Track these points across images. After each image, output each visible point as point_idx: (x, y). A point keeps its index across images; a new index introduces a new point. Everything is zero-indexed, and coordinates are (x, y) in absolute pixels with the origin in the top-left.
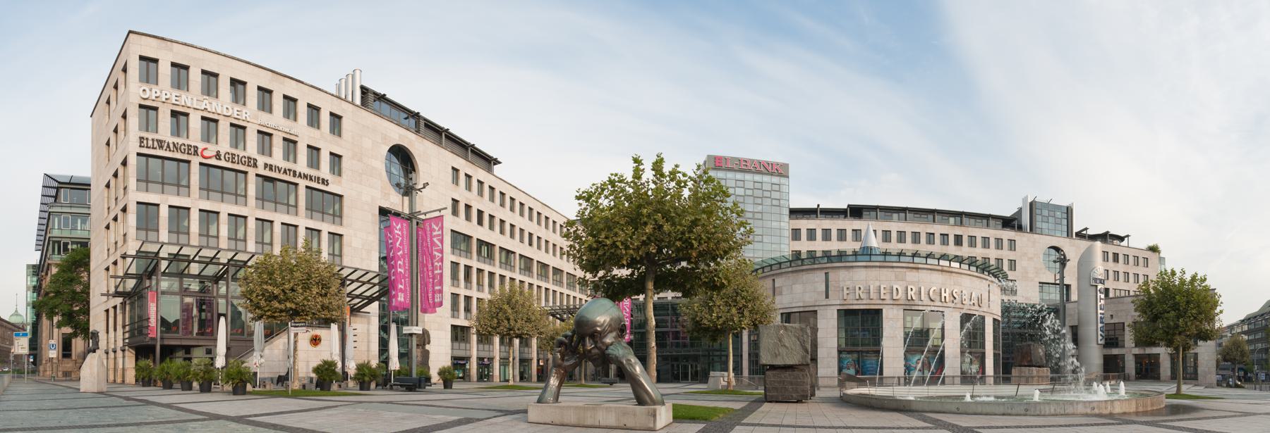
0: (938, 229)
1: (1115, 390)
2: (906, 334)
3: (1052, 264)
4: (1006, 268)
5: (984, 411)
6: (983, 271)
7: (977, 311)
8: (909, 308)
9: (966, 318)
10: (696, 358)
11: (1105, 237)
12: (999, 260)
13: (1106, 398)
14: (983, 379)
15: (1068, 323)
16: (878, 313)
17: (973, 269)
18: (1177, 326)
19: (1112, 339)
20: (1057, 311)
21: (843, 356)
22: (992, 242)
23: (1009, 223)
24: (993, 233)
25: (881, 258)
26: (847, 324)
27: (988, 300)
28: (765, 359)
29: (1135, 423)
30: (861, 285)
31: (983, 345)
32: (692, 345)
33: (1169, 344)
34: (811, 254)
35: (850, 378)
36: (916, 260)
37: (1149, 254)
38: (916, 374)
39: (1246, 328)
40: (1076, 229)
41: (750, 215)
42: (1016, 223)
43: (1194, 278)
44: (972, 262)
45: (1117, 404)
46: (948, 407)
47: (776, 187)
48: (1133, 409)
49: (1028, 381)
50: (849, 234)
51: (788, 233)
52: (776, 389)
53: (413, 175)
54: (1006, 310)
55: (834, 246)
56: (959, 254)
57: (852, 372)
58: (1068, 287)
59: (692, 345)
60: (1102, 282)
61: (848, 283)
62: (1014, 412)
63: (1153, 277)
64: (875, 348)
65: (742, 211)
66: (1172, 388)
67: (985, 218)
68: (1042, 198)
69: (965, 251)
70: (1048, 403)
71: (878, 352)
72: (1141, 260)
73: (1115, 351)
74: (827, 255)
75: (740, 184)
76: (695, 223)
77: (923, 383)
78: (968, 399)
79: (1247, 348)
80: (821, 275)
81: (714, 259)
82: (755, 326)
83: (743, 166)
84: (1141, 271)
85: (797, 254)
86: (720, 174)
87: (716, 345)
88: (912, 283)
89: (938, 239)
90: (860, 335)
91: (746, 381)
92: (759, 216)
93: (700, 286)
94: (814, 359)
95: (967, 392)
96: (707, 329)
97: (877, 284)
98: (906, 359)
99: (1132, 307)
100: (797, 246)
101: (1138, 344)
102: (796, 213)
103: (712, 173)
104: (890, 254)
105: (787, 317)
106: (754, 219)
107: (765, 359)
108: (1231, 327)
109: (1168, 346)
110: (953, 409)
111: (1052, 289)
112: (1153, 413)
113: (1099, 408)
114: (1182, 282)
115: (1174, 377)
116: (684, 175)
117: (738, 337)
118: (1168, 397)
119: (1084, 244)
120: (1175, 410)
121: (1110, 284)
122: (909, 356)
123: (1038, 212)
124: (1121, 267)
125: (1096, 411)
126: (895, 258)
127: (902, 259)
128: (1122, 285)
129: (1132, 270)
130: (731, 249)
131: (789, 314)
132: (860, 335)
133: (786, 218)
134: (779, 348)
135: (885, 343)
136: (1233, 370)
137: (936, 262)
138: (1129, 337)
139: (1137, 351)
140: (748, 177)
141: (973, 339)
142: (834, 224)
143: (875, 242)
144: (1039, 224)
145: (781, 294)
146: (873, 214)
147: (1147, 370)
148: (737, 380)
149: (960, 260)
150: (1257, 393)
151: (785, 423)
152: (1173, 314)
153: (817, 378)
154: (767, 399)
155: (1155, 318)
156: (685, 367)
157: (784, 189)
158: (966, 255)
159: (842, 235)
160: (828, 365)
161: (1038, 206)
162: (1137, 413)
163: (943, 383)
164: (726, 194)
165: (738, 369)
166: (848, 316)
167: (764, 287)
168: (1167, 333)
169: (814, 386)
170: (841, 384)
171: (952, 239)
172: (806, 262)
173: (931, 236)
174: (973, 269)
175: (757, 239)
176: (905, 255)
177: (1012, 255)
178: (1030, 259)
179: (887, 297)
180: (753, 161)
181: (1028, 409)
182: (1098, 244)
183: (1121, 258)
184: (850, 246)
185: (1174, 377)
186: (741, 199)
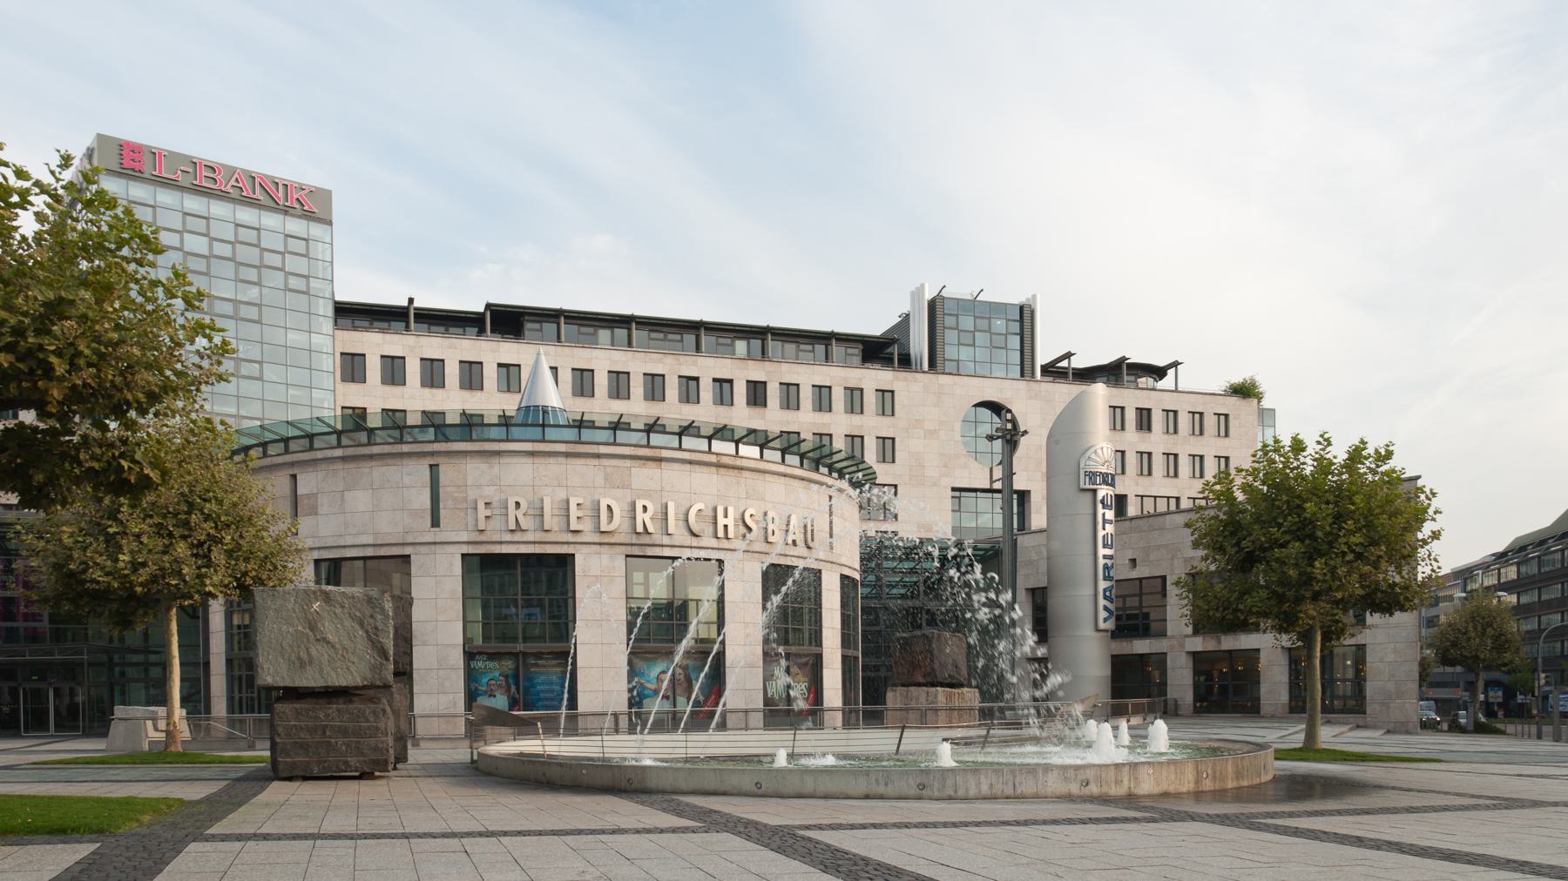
0: (708, 367)
1: (1139, 738)
2: (633, 613)
3: (984, 444)
4: (871, 456)
5: (821, 789)
6: (817, 464)
7: (801, 560)
8: (640, 551)
9: (774, 576)
10: (71, 671)
11: (1115, 372)
12: (855, 439)
13: (1121, 756)
14: (815, 713)
15: (1022, 583)
16: (564, 562)
17: (793, 460)
18: (1308, 580)
19: (1134, 614)
20: (990, 556)
21: (479, 664)
22: (838, 396)
23: (878, 350)
24: (841, 375)
25: (571, 434)
26: (487, 588)
27: (830, 533)
28: (272, 672)
29: (1193, 817)
30: (522, 497)
31: (817, 638)
32: (58, 636)
33: (1286, 623)
34: (395, 421)
35: (496, 718)
36: (656, 439)
37: (1233, 405)
38: (656, 706)
39: (1511, 573)
40: (1043, 357)
41: (228, 308)
43: (1356, 455)
44: (790, 444)
45: (1146, 772)
46: (733, 781)
47: (294, 245)
48: (1187, 785)
49: (925, 718)
50: (490, 374)
51: (330, 363)
52: (304, 747)
54: (873, 554)
55: (452, 401)
56: (757, 425)
57: (500, 702)
58: (1023, 496)
59: (58, 636)
60: (1108, 480)
61: (490, 492)
62: (890, 790)
63: (1242, 458)
64: (558, 646)
65: (200, 295)
66: (1295, 734)
67: (822, 342)
68: (959, 289)
69: (773, 418)
70: (975, 769)
71: (564, 657)
72: (1210, 422)
73: (1141, 646)
74: (434, 422)
75: (200, 225)
76: (56, 309)
77: (674, 726)
78: (781, 761)
79: (1513, 627)
81: (119, 412)
82: (244, 590)
83: (205, 180)
84: (1210, 446)
85: (356, 418)
86: (138, 191)
87: (133, 637)
88: (646, 494)
89: (707, 391)
90: (518, 615)
91: (221, 728)
92: (252, 313)
93: (77, 481)
94: (404, 673)
95: (779, 748)
96: (101, 596)
97: (562, 495)
98: (632, 672)
99: (1187, 537)
100: (355, 395)
101: (1202, 624)
103: (111, 185)
104: (592, 425)
105: (332, 570)
106: (235, 317)
107: (272, 672)
108: (1464, 575)
109: (1281, 629)
110: (747, 783)
111: (984, 502)
112: (1239, 795)
113: (1100, 781)
114: (1323, 466)
115: (1298, 705)
116: (21, 174)
117: (195, 618)
118: (1281, 755)
119: (1064, 392)
120: (1299, 788)
121: (1129, 485)
122: (639, 664)
123: (949, 321)
124: (1157, 441)
125: (1094, 789)
126: (605, 435)
127: (622, 436)
128: (1160, 485)
129: (1185, 446)
130: (168, 389)
131: (336, 564)
132: (518, 615)
133: (328, 325)
134: (309, 642)
135: (583, 634)
136: (1471, 687)
137: (702, 444)
138: (1177, 612)
139: (1198, 644)
140: (219, 209)
141: (793, 626)
142: (453, 349)
143: (554, 396)
144: (950, 352)
145: (314, 511)
146: (550, 328)
147: (1225, 690)
148: (195, 727)
149: (762, 440)
150: (1546, 746)
151: (328, 828)
152: (1296, 547)
153: (411, 720)
154: (277, 772)
155: (1247, 562)
156: (38, 696)
157: (319, 251)
158: (774, 429)
159: (472, 375)
160: (439, 686)
161: (949, 308)
162: (1198, 795)
163: (722, 726)
164: (151, 245)
165: (196, 699)
166: (490, 572)
167: (266, 492)
168: (1281, 598)
169: (404, 738)
170: (474, 731)
171: (740, 391)
172: (380, 436)
173: (690, 385)
174: (793, 460)
175: (246, 369)
176: (627, 427)
177: (885, 427)
178: (931, 434)
179: (587, 526)
180: (232, 170)
181: (926, 783)
182: (1100, 390)
183: (1157, 419)
184: (492, 402)
185: (1298, 705)
186: (193, 264)
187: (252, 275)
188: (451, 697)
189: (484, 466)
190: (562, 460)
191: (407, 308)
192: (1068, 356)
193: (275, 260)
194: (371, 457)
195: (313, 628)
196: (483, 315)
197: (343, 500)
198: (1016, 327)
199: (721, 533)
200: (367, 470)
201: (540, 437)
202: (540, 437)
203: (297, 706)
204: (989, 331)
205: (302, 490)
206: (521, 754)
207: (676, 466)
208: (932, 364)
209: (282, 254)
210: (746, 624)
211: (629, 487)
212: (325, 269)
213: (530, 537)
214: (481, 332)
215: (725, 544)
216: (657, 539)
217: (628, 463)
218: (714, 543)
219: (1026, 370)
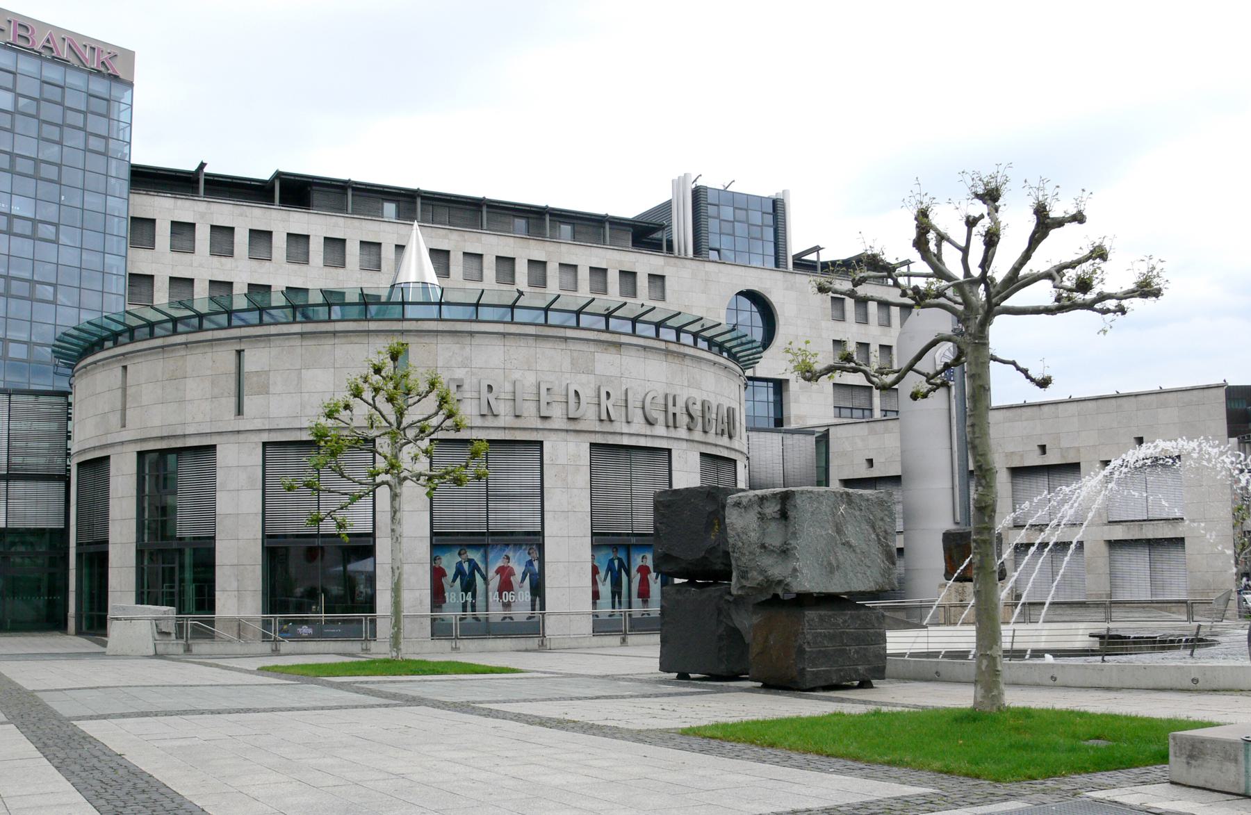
17: (703, 344)
23: (646, 233)
24: (615, 258)
40: (796, 244)
53: (629, 238)
67: (591, 227)
68: (712, 181)
75: (54, 93)
92: (51, 172)
102: (147, 179)
123: (712, 210)
142: (243, 217)
144: (714, 241)
145: (264, 390)
187: (54, 133)
188: (417, 593)
189: (456, 348)
190: (531, 341)
192: (817, 249)
193: (78, 120)
194: (335, 333)
195: (839, 531)
197: (300, 378)
198: (769, 219)
201: (436, 316)
202: (436, 316)
203: (822, 613)
205: (248, 367)
207: (633, 352)
208: (697, 251)
209: (85, 113)
211: (592, 372)
213: (501, 422)
215: (673, 433)
216: (617, 427)
217: (592, 348)
219: (779, 262)
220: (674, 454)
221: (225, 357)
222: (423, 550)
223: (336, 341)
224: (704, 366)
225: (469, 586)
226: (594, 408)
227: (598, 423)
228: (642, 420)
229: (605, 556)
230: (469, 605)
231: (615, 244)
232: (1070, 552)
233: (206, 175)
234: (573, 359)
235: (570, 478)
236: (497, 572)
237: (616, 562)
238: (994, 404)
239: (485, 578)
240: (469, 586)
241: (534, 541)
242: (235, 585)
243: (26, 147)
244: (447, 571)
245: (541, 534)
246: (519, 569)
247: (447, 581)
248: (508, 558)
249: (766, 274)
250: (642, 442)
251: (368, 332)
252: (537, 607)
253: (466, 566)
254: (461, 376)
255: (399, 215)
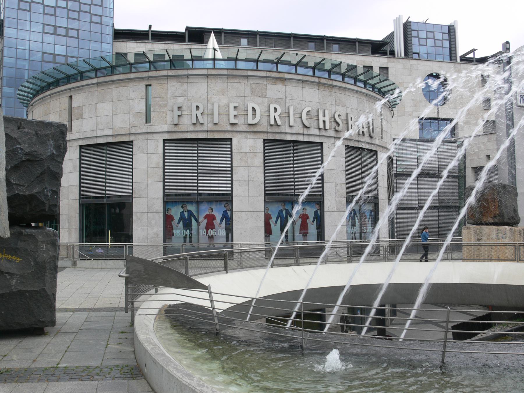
23: (378, 48)
40: (461, 51)
42: (388, 48)
68: (416, 17)
80: (141, 87)
88: (277, 101)
97: (224, 101)
102: (121, 35)
123: (414, 34)
133: (110, 38)
144: (415, 49)
145: (80, 117)
188: (155, 230)
190: (225, 79)
191: (148, 31)
192: (473, 51)
196: (183, 33)
197: (96, 108)
198: (446, 36)
199: (321, 126)
200: (109, 90)
204: (434, 38)
205: (74, 105)
206: (187, 305)
207: (294, 84)
208: (406, 54)
209: (90, 5)
210: (337, 184)
211: (265, 96)
212: (110, 13)
213: (205, 128)
214: (184, 41)
215: (324, 133)
216: (283, 129)
218: (316, 132)
220: (324, 145)
221: (65, 100)
222: (159, 205)
223: (114, 86)
224: (348, 93)
225: (187, 225)
226: (265, 118)
227: (269, 127)
228: (301, 125)
229: (275, 209)
230: (188, 237)
231: (362, 52)
232: (306, 192)
233: (152, 31)
234: (252, 88)
235: (250, 160)
236: (205, 218)
237: (284, 212)
238: (412, 29)
239: (197, 220)
240: (187, 225)
241: (226, 199)
242: (67, 225)
243: (63, 22)
244: (175, 217)
245: (231, 194)
246: (218, 216)
247: (174, 223)
248: (212, 209)
249: (444, 64)
250: (301, 138)
251: (130, 79)
252: (230, 239)
253: (186, 214)
254: (181, 101)
255: (249, 44)
